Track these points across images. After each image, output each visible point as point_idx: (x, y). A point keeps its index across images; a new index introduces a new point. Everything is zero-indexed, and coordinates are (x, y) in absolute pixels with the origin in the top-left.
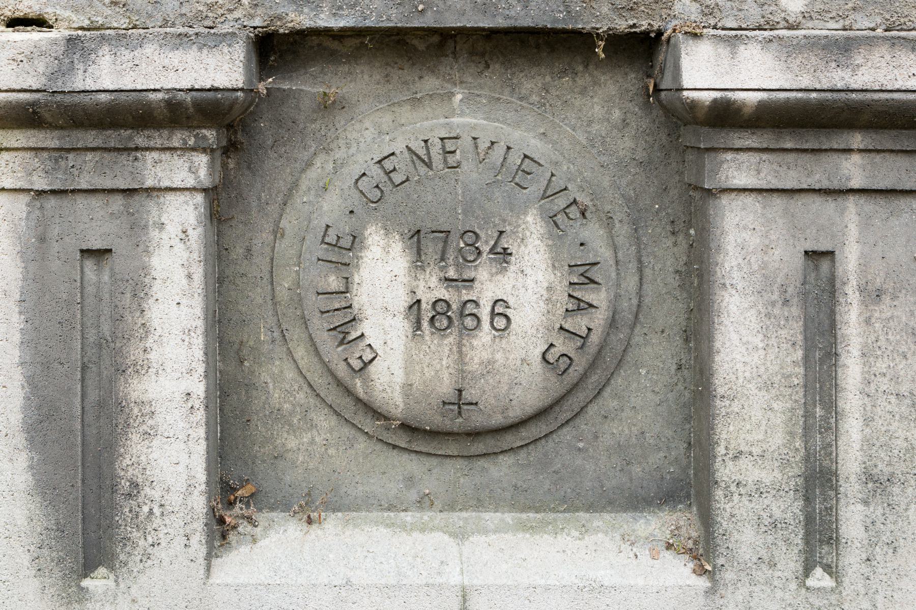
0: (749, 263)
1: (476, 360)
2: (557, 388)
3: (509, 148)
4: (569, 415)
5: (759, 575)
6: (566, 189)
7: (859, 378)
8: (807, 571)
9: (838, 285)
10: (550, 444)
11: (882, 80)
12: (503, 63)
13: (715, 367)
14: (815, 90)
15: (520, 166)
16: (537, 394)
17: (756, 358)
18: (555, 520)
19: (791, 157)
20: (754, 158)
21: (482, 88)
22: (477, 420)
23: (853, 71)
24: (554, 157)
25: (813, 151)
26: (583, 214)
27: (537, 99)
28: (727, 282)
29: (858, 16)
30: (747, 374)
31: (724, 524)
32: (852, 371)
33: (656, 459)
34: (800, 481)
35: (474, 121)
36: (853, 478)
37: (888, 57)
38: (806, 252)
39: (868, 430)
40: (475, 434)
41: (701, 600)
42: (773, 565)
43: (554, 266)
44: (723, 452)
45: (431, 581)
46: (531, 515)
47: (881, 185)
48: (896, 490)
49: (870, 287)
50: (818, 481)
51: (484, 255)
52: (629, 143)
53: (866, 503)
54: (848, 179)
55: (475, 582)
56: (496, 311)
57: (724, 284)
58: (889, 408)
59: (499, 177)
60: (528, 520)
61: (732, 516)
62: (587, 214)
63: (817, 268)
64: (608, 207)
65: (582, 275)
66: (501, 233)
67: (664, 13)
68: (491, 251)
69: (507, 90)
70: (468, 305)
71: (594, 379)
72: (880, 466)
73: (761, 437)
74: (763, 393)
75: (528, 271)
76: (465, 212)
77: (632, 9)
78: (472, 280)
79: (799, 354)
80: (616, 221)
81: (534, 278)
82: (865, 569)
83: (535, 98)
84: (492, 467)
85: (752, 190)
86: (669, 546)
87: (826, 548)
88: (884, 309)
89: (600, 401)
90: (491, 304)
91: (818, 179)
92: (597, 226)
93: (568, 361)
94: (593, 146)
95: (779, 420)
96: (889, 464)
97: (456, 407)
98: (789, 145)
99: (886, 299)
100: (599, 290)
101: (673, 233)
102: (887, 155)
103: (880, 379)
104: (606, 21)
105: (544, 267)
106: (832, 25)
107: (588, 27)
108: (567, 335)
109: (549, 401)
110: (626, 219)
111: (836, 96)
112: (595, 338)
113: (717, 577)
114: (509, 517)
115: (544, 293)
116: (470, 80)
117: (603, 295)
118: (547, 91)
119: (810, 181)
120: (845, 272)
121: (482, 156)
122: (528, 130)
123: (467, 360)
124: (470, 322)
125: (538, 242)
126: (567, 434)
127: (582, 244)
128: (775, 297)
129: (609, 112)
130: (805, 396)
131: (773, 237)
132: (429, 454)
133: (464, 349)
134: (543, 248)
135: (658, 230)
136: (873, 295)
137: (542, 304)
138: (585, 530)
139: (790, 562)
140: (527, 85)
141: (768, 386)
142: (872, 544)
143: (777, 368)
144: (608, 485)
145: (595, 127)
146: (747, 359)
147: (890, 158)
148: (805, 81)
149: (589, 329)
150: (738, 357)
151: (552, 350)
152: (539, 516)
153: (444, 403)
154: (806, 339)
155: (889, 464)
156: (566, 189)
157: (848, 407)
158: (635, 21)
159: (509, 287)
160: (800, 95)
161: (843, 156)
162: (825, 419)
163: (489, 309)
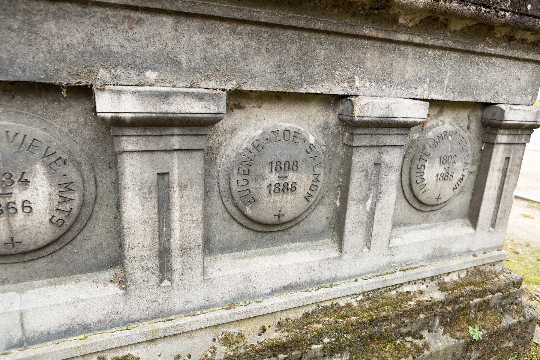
0: (135, 179)
1: (17, 225)
2: (58, 232)
3: (25, 136)
4: (68, 241)
5: (143, 286)
6: (55, 153)
7: (178, 216)
8: (161, 281)
9: (170, 184)
10: (62, 252)
11: (180, 109)
12: (22, 96)
13: (123, 218)
14: (154, 113)
15: (31, 144)
16: (50, 235)
17: (139, 213)
18: (66, 279)
19: (150, 138)
20: (135, 139)
21: (12, 107)
22: (23, 248)
23: (169, 105)
24: (49, 139)
25: (159, 135)
26: (65, 163)
27: (42, 113)
28: (127, 187)
29: (178, 82)
30: (136, 219)
31: (129, 271)
32: (176, 214)
33: (107, 252)
34: (157, 253)
35: (7, 123)
36: (177, 250)
37: (183, 100)
38: (158, 174)
39: (182, 233)
40: (25, 253)
41: (122, 297)
42: (148, 281)
43: (51, 185)
44: (128, 247)
45: (6, 311)
46: (56, 279)
47: (186, 148)
48: (192, 251)
49: (182, 185)
50: (164, 253)
51: (16, 183)
52: (88, 132)
53: (181, 257)
54: (173, 146)
55: (26, 308)
56: (25, 205)
57: (125, 188)
58: (189, 225)
59: (21, 149)
60: (54, 281)
61: (132, 268)
62: (66, 163)
63: (163, 179)
64: (78, 159)
65: (66, 187)
66: (24, 173)
67: (94, 77)
68: (19, 181)
69: (25, 109)
70: (10, 204)
71: (77, 226)
72: (186, 244)
73: (142, 240)
74: (143, 225)
75: (39, 188)
76: (4, 165)
77: (78, 75)
78: (11, 194)
79: (156, 210)
80: (83, 165)
81: (42, 191)
82: (181, 278)
83: (40, 112)
84: (36, 264)
85: (135, 151)
86: (111, 281)
87: (168, 273)
88: (188, 192)
89: (82, 234)
90: (21, 203)
91: (162, 146)
92: (72, 167)
93: (63, 221)
94: (71, 133)
95: (149, 234)
96: (189, 243)
97: (11, 245)
98: (149, 134)
99: (189, 188)
100: (74, 193)
101: (110, 168)
102: (188, 136)
103: (186, 216)
104: (66, 80)
105: (46, 186)
106: (168, 85)
107: (57, 82)
108: (60, 212)
109: (56, 237)
110: (87, 163)
111: (162, 115)
112: (74, 212)
113: (128, 289)
114: (45, 281)
115: (48, 196)
116: (5, 103)
117: (76, 194)
118: (46, 109)
119: (158, 147)
120: (173, 180)
121: (11, 140)
122: (37, 127)
123: (13, 226)
124: (12, 211)
125: (42, 176)
126: (69, 247)
127: (64, 175)
128: (146, 191)
129: (77, 118)
130: (159, 224)
131: (145, 169)
132: (4, 263)
133: (11, 222)
134: (45, 178)
135: (103, 167)
136: (183, 187)
137: (47, 201)
138: (78, 280)
139: (154, 280)
140: (36, 107)
141: (144, 223)
142: (183, 269)
143: (147, 216)
144: (88, 263)
145: (71, 125)
146: (136, 214)
147: (189, 137)
148: (150, 109)
149: (71, 209)
150: (132, 213)
151: (54, 218)
152: (59, 279)
153: (5, 244)
154: (159, 205)
155: (189, 243)
156: (55, 153)
157: (174, 227)
158: (80, 80)
159: (29, 195)
160: (148, 115)
161: (171, 137)
162: (167, 231)
163: (20, 205)
